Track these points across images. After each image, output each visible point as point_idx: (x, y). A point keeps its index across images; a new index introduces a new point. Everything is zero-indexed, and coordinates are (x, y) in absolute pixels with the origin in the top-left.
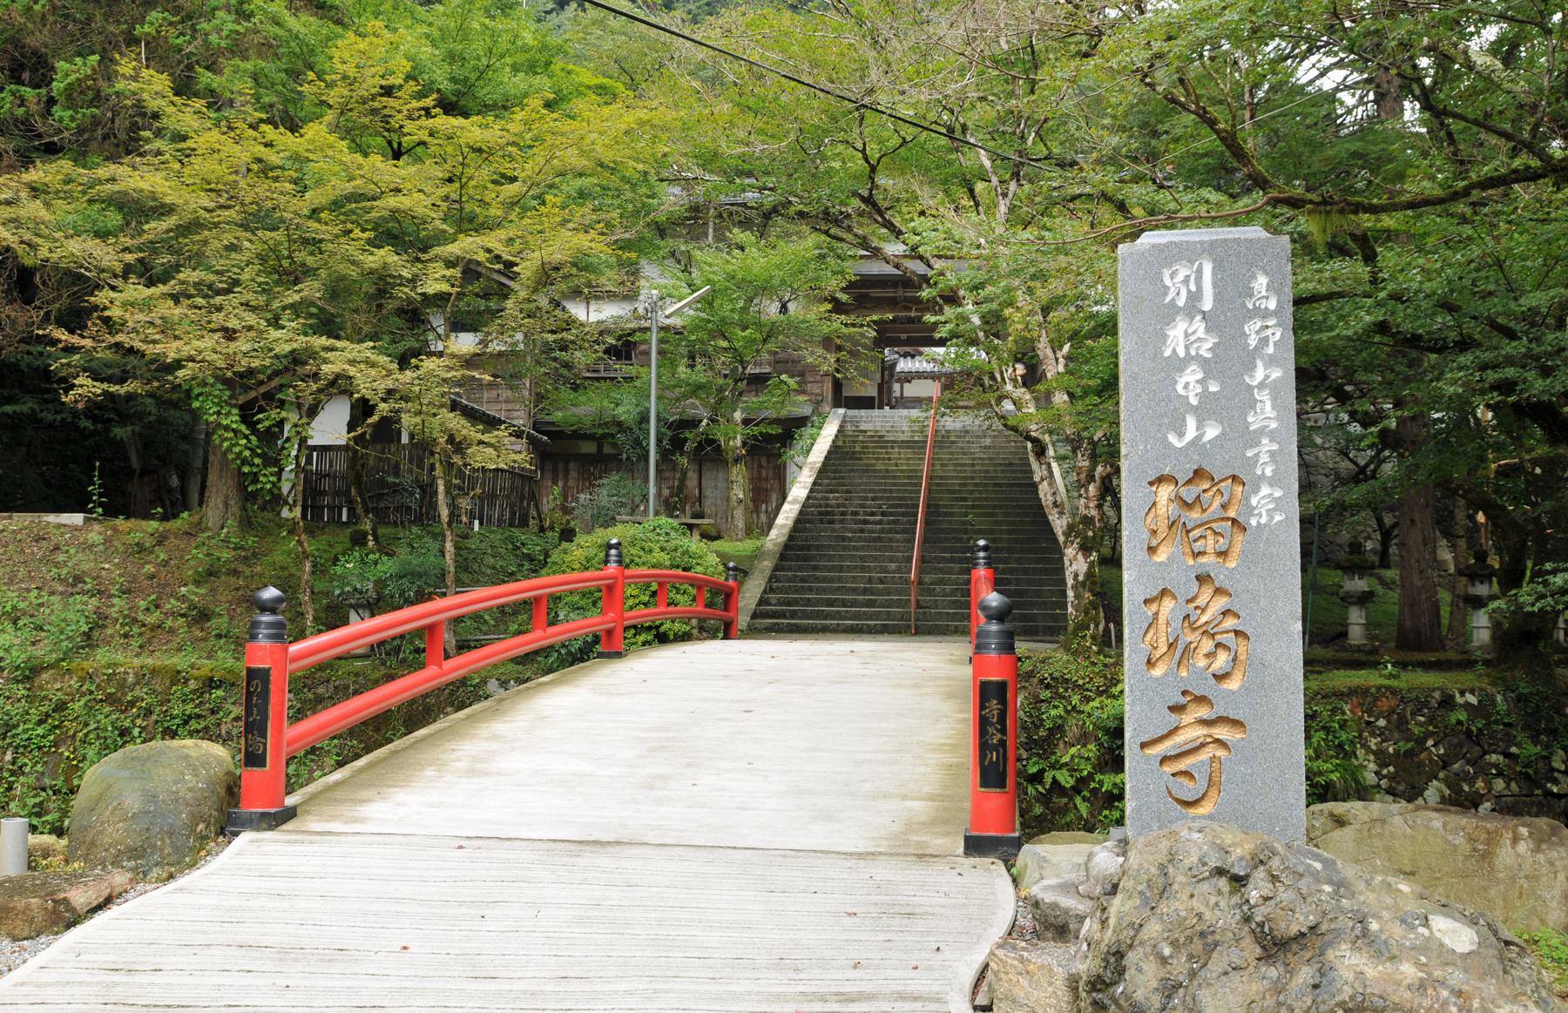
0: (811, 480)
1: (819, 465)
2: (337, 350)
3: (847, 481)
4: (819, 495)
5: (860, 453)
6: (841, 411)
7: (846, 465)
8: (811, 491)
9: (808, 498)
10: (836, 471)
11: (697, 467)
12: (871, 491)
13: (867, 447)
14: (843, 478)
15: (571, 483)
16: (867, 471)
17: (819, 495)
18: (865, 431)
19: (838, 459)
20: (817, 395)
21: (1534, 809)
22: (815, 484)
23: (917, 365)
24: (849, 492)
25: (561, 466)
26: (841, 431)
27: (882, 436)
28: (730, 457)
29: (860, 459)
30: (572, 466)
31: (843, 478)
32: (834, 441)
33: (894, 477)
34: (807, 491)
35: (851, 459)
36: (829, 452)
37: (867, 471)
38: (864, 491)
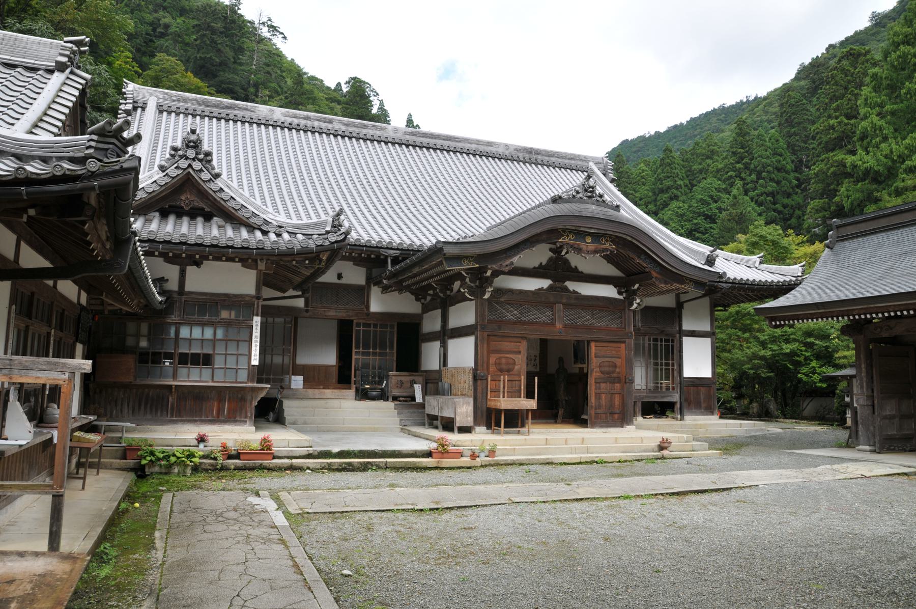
23: (215, 232)
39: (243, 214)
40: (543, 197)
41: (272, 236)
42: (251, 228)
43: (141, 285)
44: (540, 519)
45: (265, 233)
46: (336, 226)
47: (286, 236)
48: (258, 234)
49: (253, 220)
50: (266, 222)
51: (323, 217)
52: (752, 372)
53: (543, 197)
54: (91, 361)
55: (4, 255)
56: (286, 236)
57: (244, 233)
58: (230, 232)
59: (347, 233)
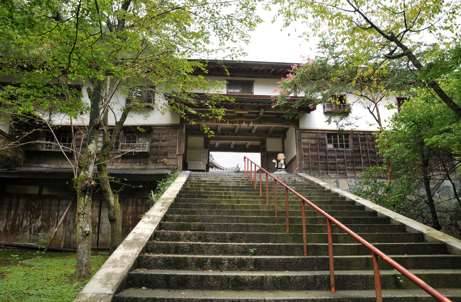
0: (161, 214)
1: (171, 201)
2: (133, 202)
3: (198, 216)
4: (169, 233)
5: (205, 193)
6: (188, 172)
7: (195, 201)
8: (160, 226)
9: (155, 236)
10: (186, 206)
11: (98, 204)
12: (227, 228)
13: (208, 190)
14: (193, 212)
15: (19, 212)
16: (215, 206)
17: (169, 233)
18: (205, 181)
19: (188, 196)
20: (174, 165)
21: (251, 255)
22: (165, 218)
23: (214, 170)
24: (201, 228)
25: (14, 201)
26: (188, 180)
27: (218, 184)
28: (79, 187)
29: (206, 197)
30: (22, 201)
31: (193, 212)
32: (184, 185)
33: (242, 213)
34: (154, 227)
35: (198, 197)
36: (180, 192)
37: (215, 206)
38: (219, 227)
39: (219, 166)
40: (232, 165)
41: (225, 170)
42: (221, 169)
43: (130, 160)
44: (410, 100)
45: (224, 170)
46: (237, 167)
47: (228, 170)
48: (222, 170)
49: (221, 167)
50: (224, 168)
51: (235, 166)
52: (104, 95)
53: (232, 165)
54: (43, 193)
55: (211, 77)
56: (228, 170)
57: (220, 170)
58: (217, 170)
59: (240, 169)
